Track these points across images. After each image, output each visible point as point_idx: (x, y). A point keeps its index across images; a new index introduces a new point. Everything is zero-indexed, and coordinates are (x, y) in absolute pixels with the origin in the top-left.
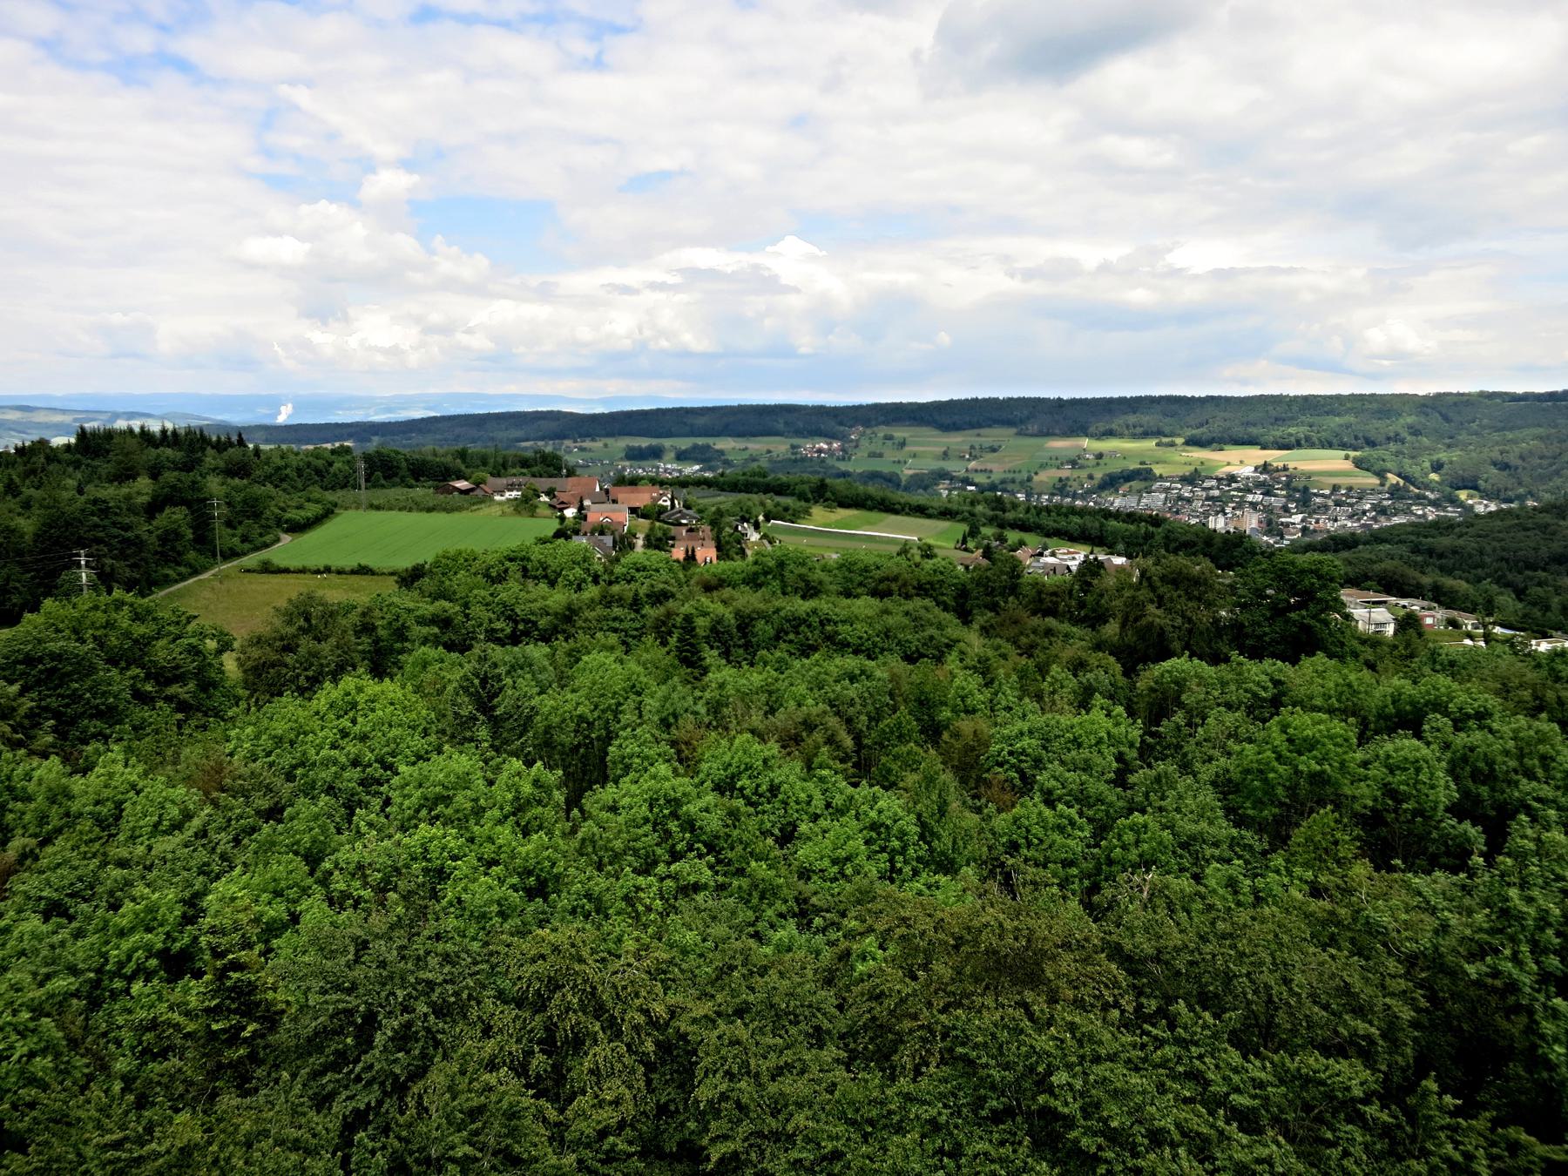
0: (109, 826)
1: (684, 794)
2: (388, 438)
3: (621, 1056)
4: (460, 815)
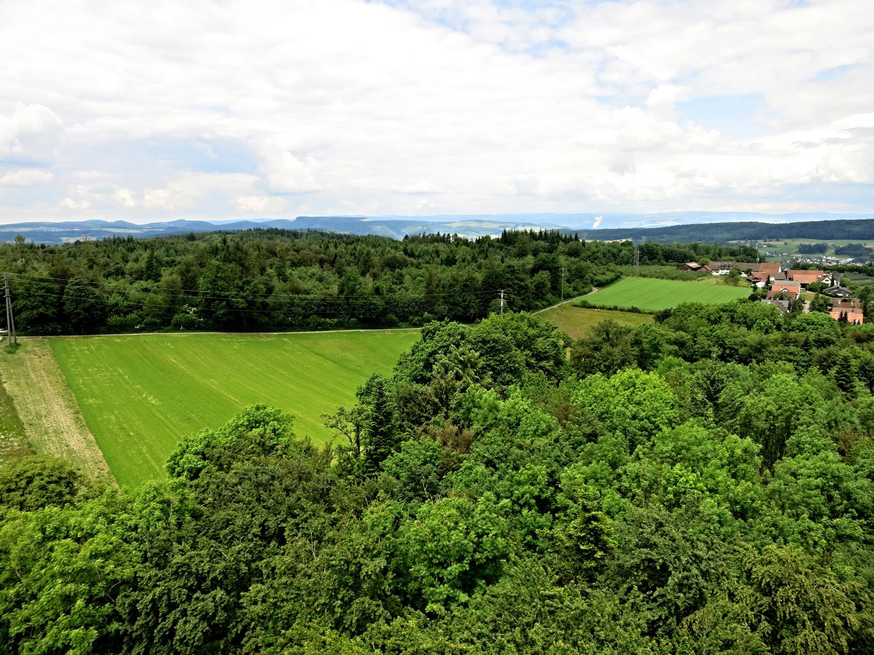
0: (513, 427)
1: (846, 475)
2: (651, 237)
3: (822, 642)
4: (694, 458)
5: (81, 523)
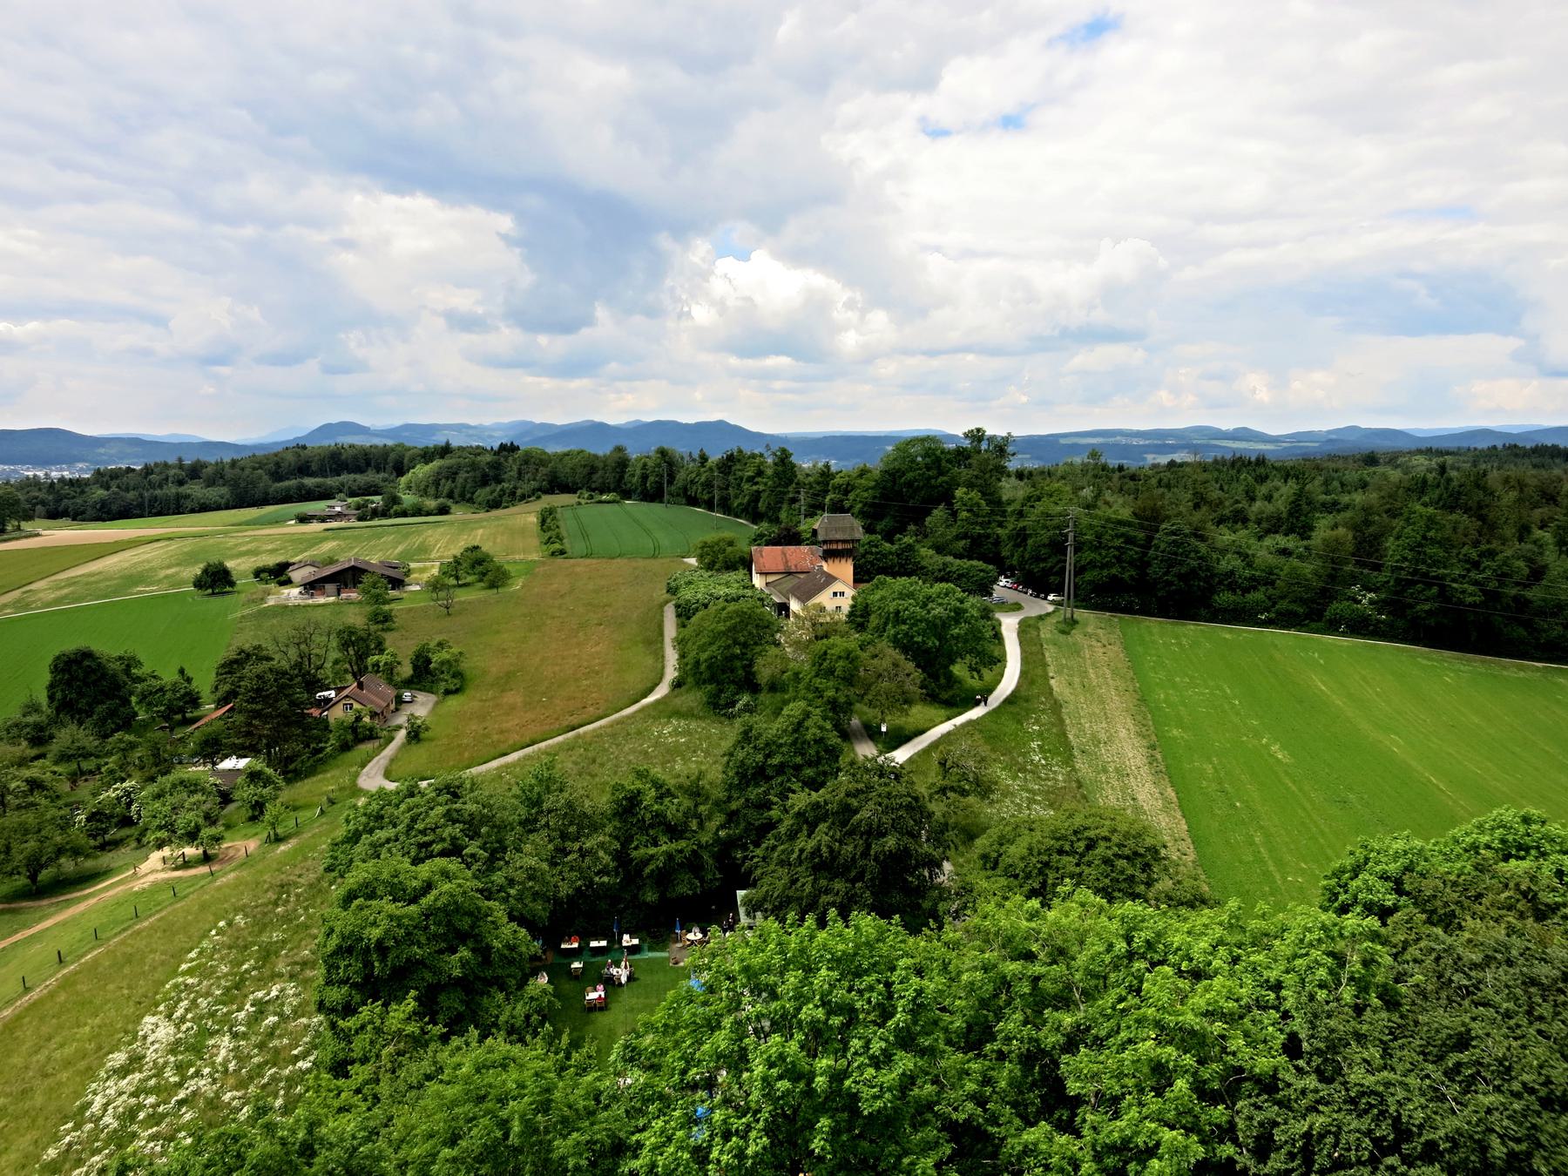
5: (1190, 947)
